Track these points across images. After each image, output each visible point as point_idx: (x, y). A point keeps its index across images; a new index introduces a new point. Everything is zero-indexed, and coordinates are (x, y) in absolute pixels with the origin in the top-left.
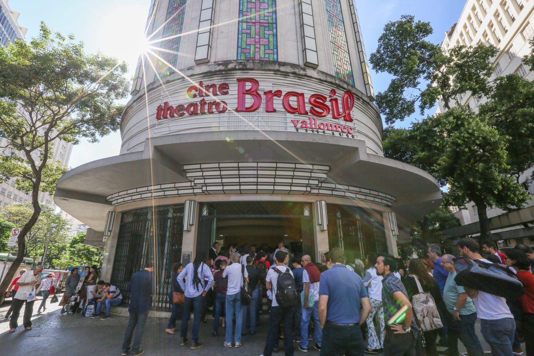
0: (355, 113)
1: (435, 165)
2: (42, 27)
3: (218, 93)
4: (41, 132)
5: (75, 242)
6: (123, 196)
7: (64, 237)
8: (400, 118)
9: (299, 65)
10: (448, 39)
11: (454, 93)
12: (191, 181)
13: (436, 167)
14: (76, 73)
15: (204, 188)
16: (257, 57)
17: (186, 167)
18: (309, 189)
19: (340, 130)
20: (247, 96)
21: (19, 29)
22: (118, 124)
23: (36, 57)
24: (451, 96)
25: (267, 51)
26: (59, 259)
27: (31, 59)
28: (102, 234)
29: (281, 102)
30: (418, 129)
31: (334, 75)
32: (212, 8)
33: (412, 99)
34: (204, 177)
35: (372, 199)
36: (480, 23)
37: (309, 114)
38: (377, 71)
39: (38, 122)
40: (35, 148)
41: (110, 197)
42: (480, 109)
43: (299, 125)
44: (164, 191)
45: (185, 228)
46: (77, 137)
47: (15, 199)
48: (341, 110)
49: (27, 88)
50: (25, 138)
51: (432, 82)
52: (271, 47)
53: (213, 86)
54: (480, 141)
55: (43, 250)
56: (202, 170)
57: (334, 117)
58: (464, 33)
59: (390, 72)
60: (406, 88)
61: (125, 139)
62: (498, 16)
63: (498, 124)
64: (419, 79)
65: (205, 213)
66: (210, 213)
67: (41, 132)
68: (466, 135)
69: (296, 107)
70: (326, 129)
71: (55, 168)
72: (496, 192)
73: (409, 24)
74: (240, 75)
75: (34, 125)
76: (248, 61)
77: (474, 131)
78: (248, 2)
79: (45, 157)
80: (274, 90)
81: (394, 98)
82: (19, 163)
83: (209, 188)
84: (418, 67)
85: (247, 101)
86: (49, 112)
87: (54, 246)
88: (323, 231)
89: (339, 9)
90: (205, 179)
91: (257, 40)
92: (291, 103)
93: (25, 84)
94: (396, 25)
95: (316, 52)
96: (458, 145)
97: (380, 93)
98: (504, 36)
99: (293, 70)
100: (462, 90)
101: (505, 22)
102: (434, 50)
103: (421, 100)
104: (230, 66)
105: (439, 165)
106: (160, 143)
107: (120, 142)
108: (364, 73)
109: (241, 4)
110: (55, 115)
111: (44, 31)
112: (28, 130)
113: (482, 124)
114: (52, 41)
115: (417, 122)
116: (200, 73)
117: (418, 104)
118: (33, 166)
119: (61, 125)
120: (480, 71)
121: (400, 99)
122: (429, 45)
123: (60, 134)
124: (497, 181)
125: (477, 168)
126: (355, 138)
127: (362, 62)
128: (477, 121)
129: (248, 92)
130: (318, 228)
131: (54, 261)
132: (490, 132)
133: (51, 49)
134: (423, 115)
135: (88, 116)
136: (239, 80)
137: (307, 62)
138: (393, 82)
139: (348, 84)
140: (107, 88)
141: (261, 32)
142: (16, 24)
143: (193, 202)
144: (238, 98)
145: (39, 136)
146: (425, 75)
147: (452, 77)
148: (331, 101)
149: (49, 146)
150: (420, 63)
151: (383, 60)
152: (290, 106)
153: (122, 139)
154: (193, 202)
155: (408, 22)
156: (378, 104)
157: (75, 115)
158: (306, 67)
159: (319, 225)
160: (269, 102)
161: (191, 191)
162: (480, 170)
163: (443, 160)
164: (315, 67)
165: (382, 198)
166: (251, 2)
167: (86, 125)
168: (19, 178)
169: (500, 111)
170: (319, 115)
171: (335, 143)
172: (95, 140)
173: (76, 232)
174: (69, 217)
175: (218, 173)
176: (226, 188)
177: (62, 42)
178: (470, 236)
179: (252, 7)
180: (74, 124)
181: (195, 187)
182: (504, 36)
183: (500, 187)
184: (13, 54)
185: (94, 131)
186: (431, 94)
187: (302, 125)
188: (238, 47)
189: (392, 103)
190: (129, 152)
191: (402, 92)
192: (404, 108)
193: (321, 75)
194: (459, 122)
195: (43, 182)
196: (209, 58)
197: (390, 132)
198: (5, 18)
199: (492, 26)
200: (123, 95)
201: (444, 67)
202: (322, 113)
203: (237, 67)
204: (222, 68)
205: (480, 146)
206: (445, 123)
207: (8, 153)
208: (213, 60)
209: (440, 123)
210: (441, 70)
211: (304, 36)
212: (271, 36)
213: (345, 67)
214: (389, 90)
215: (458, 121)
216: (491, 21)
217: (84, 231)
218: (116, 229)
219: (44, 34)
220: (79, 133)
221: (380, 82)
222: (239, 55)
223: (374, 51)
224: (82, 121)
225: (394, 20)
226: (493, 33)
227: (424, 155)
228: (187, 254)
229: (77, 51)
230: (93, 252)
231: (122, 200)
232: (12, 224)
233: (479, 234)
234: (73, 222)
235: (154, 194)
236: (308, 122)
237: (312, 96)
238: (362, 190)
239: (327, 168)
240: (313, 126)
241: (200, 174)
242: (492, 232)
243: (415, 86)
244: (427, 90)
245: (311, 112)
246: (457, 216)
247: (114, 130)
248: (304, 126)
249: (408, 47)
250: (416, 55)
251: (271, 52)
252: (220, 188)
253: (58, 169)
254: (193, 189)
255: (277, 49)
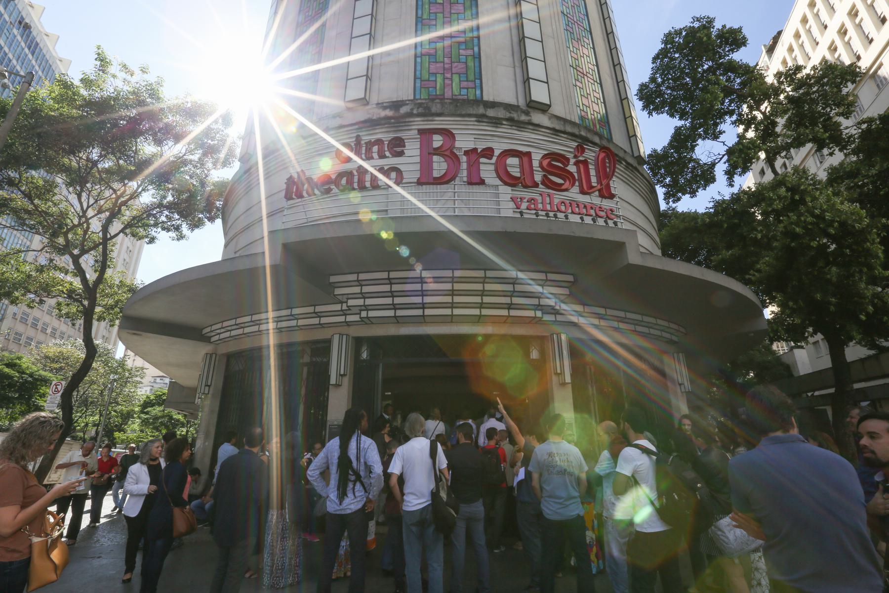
0: (617, 186)
1: (752, 272)
2: (99, 54)
3: (387, 154)
4: (96, 225)
5: (147, 404)
6: (229, 328)
7: (129, 399)
8: (690, 193)
9: (518, 106)
10: (766, 58)
11: (787, 147)
12: (342, 303)
13: (754, 275)
14: (151, 128)
15: (364, 314)
16: (448, 94)
17: (333, 279)
18: (539, 314)
19: (592, 212)
20: (435, 158)
21: (58, 62)
22: (218, 209)
23: (89, 104)
24: (779, 153)
25: (464, 84)
26: (124, 431)
27: (81, 106)
28: (193, 391)
29: (492, 168)
30: (724, 210)
31: (577, 121)
32: (372, 15)
33: (710, 160)
34: (364, 296)
35: (645, 330)
36: (823, 28)
37: (541, 186)
38: (650, 114)
39: (90, 209)
40: (87, 252)
41: (208, 329)
42: (829, 173)
43: (524, 206)
44: (252, 321)
45: (333, 381)
46: (153, 232)
47: (53, 335)
48: (594, 180)
49: (74, 154)
50: (70, 236)
51: (746, 130)
52: (471, 77)
53: (379, 142)
54: (835, 229)
55: (97, 417)
56: (360, 283)
57: (583, 192)
58: (795, 47)
59: (672, 116)
60: (700, 141)
61: (230, 235)
62: (856, 15)
63: (863, 200)
64: (722, 125)
65: (365, 355)
66: (371, 354)
67: (96, 225)
68: (810, 219)
69: (518, 175)
70: (570, 211)
71: (117, 282)
72: (863, 317)
73: (705, 31)
74: (420, 123)
75: (84, 212)
76: (433, 100)
77: (823, 211)
78: (430, 3)
79: (103, 265)
80: (481, 146)
81: (680, 158)
82: (62, 276)
83: (372, 314)
84: (722, 104)
85: (435, 166)
86: (107, 193)
87: (115, 411)
88: (563, 384)
89: (583, 11)
90: (364, 298)
91: (446, 66)
92: (509, 169)
93: (70, 146)
94: (684, 34)
95: (547, 83)
96: (795, 236)
97: (655, 151)
98: (866, 49)
99: (508, 115)
100: (798, 143)
101: (869, 26)
102: (750, 74)
103: (728, 161)
104: (404, 110)
105: (759, 271)
106: (293, 238)
107: (222, 242)
108: (627, 118)
109: (420, 7)
110: (118, 198)
111: (102, 61)
112: (76, 222)
113: (838, 200)
114: (114, 76)
115: (721, 198)
116: (354, 122)
117: (720, 169)
118: (84, 280)
119: (127, 214)
120: (832, 109)
121: (691, 160)
122: (740, 66)
123: (125, 228)
124: (865, 298)
125: (828, 276)
126: (619, 225)
127: (623, 99)
128: (828, 195)
129: (438, 151)
130: (555, 379)
131: (117, 434)
132: (852, 214)
133: (112, 90)
134: (732, 186)
135: (170, 198)
136: (421, 132)
137: (531, 101)
138: (678, 130)
139: (601, 137)
140: (200, 151)
141: (453, 53)
142: (54, 54)
143: (345, 337)
144: (421, 163)
145: (93, 232)
146: (734, 117)
147: (781, 121)
148: (576, 164)
149: (109, 247)
150: (726, 96)
151: (660, 94)
152: (508, 173)
153: (225, 234)
154: (345, 337)
155: (704, 27)
156: (651, 169)
157: (147, 198)
158: (530, 110)
159: (556, 374)
160: (473, 167)
161: (342, 319)
162: (834, 279)
163: (766, 262)
164: (545, 108)
165: (662, 328)
166: (436, 3)
167: (166, 213)
168: (60, 299)
169: (867, 177)
170: (558, 188)
171: (585, 235)
172: (181, 237)
173: (148, 389)
174: (139, 362)
175: (387, 288)
176: (400, 313)
177: (129, 77)
178: (810, 394)
179: (438, 11)
180: (148, 211)
181: (349, 312)
182: (866, 49)
183: (870, 309)
184: (52, 99)
185: (179, 222)
186: (745, 151)
187: (529, 205)
188: (415, 78)
189: (677, 167)
190: (237, 255)
191: (693, 149)
192: (697, 176)
193: (556, 121)
194: (797, 197)
195: (99, 305)
196: (367, 98)
197: (670, 217)
198: (37, 44)
199: (845, 33)
200: (226, 163)
201: (766, 104)
202: (562, 185)
203: (415, 112)
204: (389, 113)
205: (833, 238)
206: (771, 199)
207: (43, 261)
208: (374, 99)
209: (763, 199)
210: (763, 108)
211: (526, 57)
212: (470, 58)
213: (596, 108)
214: (671, 144)
215: (791, 193)
216: (843, 25)
217: (163, 386)
218: (218, 382)
219: (102, 66)
220: (156, 225)
221: (654, 132)
222: (418, 92)
223: (646, 79)
224: (160, 205)
225: (679, 26)
226: (848, 44)
227: (732, 255)
228: (336, 423)
229: (154, 94)
230: (178, 420)
231: (227, 334)
232: (50, 375)
233: (832, 390)
234: (144, 372)
235: (301, 322)
236: (539, 199)
237: (545, 157)
238: (629, 315)
239: (570, 278)
240: (548, 207)
241: (357, 290)
242: (857, 386)
243: (715, 137)
244: (737, 144)
245: (543, 183)
246: (786, 360)
247: (212, 219)
248: (533, 206)
249: (704, 71)
250: (718, 84)
251: (471, 84)
252: (391, 313)
253: (122, 284)
254: (345, 315)
255: (481, 79)
